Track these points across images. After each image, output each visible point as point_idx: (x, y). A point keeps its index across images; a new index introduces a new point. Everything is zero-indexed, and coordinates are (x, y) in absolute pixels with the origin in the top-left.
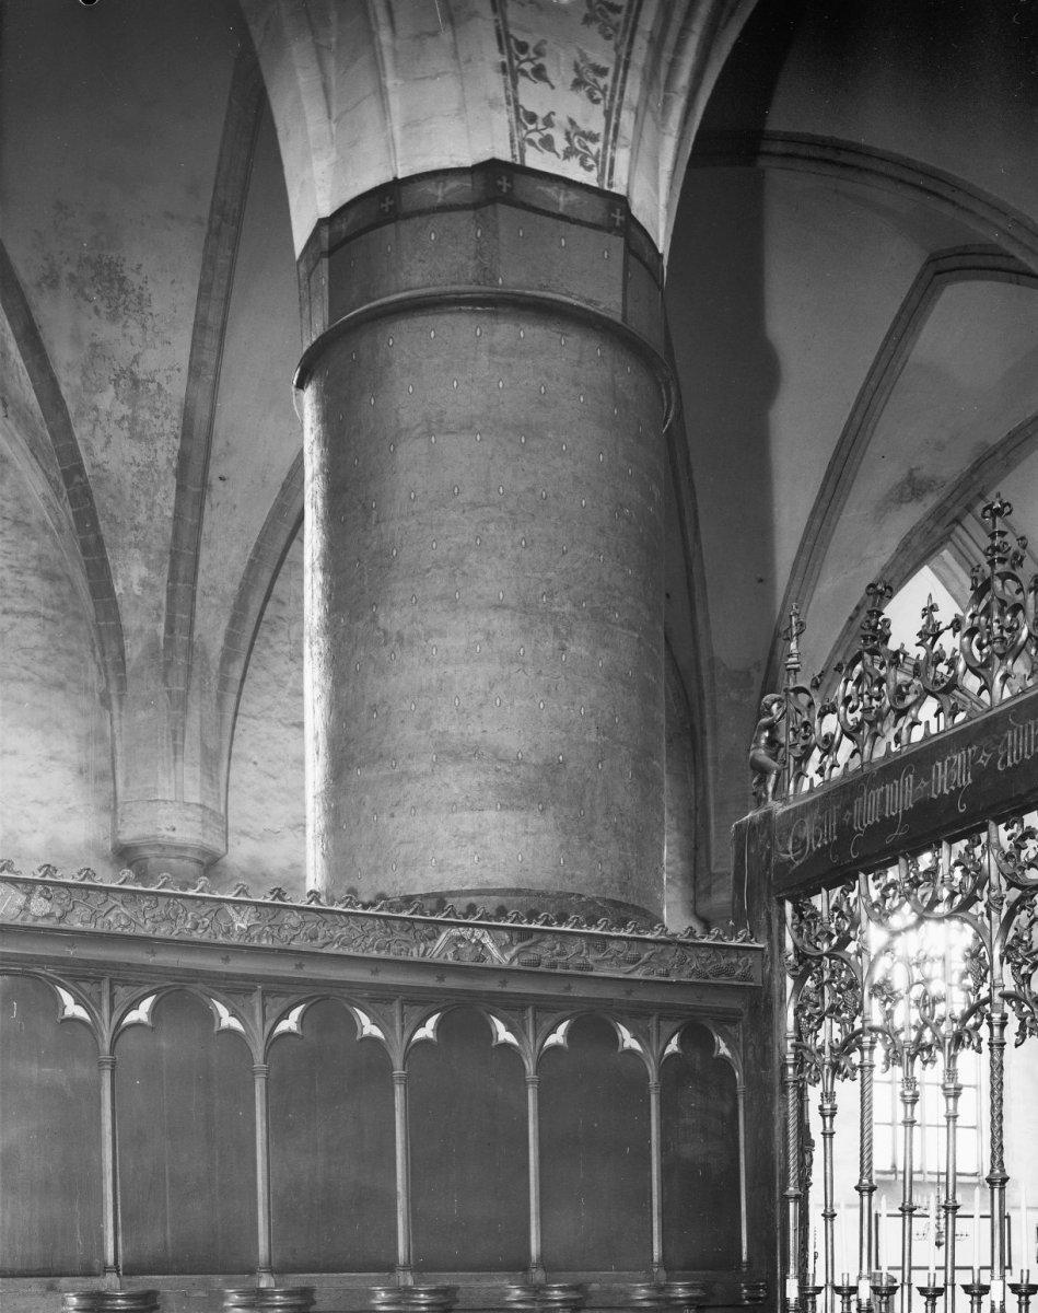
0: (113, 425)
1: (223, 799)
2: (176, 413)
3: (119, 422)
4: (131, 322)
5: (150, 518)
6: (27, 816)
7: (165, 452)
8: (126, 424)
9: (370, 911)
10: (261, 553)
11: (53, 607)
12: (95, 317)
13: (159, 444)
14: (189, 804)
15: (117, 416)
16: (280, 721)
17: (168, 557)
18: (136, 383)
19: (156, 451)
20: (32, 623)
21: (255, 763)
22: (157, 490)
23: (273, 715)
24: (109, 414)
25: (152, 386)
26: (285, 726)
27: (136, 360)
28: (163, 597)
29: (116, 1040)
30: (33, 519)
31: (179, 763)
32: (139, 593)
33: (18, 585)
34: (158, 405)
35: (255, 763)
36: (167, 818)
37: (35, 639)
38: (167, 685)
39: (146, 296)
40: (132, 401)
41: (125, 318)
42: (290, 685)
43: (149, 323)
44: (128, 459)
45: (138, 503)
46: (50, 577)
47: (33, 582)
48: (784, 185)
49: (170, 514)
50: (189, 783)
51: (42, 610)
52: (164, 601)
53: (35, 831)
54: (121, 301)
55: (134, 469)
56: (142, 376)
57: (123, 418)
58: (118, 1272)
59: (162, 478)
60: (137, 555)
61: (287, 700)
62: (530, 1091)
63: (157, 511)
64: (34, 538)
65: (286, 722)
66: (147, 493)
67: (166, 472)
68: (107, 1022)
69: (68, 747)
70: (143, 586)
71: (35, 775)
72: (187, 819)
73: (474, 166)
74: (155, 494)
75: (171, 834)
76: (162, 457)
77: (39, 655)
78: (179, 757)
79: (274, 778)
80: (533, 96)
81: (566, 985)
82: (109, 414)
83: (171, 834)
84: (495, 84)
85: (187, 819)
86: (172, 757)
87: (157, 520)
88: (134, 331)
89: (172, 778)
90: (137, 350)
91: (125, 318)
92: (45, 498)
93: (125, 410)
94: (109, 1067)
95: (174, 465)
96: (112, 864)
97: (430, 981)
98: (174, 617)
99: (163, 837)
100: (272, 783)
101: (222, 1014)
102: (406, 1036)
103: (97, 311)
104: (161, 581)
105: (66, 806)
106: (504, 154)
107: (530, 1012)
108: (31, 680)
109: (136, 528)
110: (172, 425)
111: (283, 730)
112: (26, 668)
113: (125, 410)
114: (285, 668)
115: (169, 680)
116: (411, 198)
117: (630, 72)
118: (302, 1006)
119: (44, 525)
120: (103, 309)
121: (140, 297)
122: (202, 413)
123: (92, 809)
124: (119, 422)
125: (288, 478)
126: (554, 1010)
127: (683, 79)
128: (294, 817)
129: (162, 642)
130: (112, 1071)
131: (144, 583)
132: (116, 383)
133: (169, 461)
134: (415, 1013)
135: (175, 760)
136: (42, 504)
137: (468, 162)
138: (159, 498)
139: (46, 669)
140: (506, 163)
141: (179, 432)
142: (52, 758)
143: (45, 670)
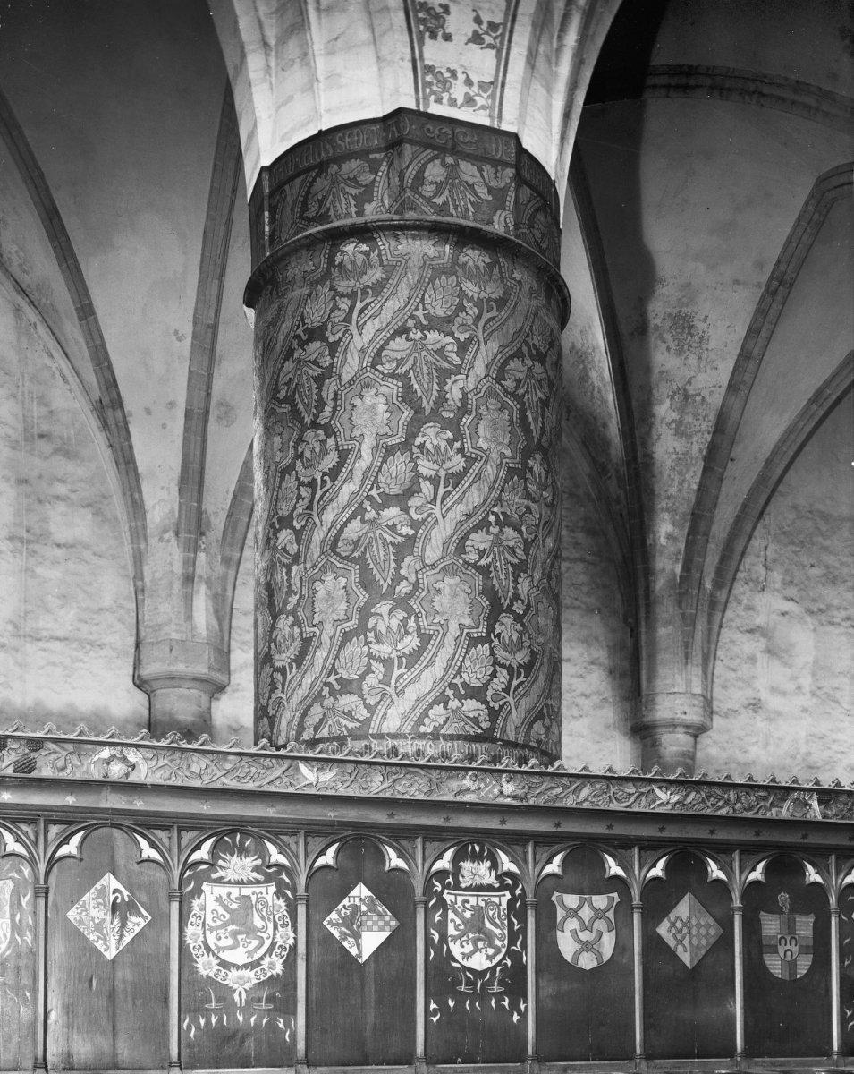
0: (664, 426)
1: (709, 689)
2: (712, 417)
3: (669, 425)
4: (692, 356)
5: (680, 490)
6: (577, 705)
7: (698, 445)
8: (674, 425)
9: (282, 752)
10: (746, 510)
11: (594, 554)
12: (666, 353)
13: (694, 439)
14: (695, 695)
15: (668, 420)
16: (738, 628)
17: (689, 518)
18: (686, 396)
19: (692, 443)
20: (580, 567)
21: (722, 661)
22: (688, 470)
23: (734, 625)
24: (663, 419)
25: (698, 399)
26: (741, 632)
27: (689, 382)
28: (682, 545)
29: (50, 871)
30: (581, 492)
31: (689, 666)
32: (665, 544)
33: (570, 539)
34: (700, 411)
35: (722, 661)
36: (681, 705)
37: (583, 578)
38: (681, 609)
39: (706, 337)
40: (682, 410)
41: (688, 352)
42: (745, 602)
43: (704, 356)
44: (671, 450)
45: (673, 480)
46: (591, 532)
47: (581, 536)
48: (660, 114)
49: (695, 487)
50: (694, 679)
51: (587, 557)
52: (683, 549)
53: (581, 716)
54: (688, 341)
55: (674, 456)
56: (691, 392)
57: (672, 422)
58: (180, 1067)
59: (694, 462)
60: (666, 517)
61: (743, 613)
62: (529, 912)
63: (686, 485)
64: (581, 505)
65: (741, 629)
66: (680, 473)
67: (697, 457)
68: (42, 859)
69: (601, 654)
70: (668, 538)
71: (581, 676)
72: (694, 706)
73: (384, 117)
74: (686, 473)
75: (684, 717)
76: (696, 447)
77: (585, 589)
78: (689, 660)
79: (734, 671)
80: (434, 53)
81: (445, 816)
82: (663, 419)
83: (684, 717)
84: (398, 43)
85: (694, 706)
86: (684, 661)
87: (684, 494)
88: (693, 360)
89: (684, 676)
90: (692, 374)
91: (688, 352)
92: (589, 476)
93: (675, 416)
94: (178, 899)
95: (704, 453)
96: (630, 738)
97: (331, 814)
98: (691, 561)
99: (678, 719)
100: (733, 675)
101: (271, 852)
102: (427, 865)
103: (668, 349)
104: (682, 535)
105: (601, 698)
106: (410, 104)
107: (419, 840)
108: (579, 607)
109: (668, 498)
110: (707, 425)
111: (740, 635)
112: (576, 599)
113: (675, 416)
114: (742, 589)
115: (683, 605)
116: (345, 143)
117: (517, 27)
118: (214, 838)
119: (588, 495)
120: (673, 345)
121: (701, 338)
122: (735, 415)
123: (618, 699)
124: (669, 425)
125: (771, 455)
126: (550, 844)
127: (572, 38)
128: (747, 699)
129: (678, 578)
130: (180, 902)
131: (669, 536)
132: (672, 397)
133: (701, 451)
134: (433, 847)
135: (687, 663)
136: (587, 480)
137: (380, 115)
138: (688, 476)
139: (589, 600)
140: (412, 110)
141: (711, 430)
142: (592, 663)
143: (588, 600)
